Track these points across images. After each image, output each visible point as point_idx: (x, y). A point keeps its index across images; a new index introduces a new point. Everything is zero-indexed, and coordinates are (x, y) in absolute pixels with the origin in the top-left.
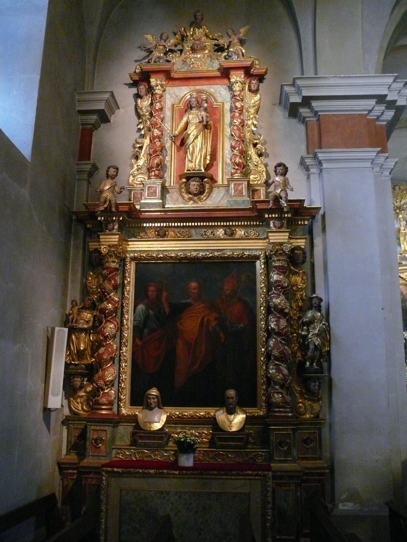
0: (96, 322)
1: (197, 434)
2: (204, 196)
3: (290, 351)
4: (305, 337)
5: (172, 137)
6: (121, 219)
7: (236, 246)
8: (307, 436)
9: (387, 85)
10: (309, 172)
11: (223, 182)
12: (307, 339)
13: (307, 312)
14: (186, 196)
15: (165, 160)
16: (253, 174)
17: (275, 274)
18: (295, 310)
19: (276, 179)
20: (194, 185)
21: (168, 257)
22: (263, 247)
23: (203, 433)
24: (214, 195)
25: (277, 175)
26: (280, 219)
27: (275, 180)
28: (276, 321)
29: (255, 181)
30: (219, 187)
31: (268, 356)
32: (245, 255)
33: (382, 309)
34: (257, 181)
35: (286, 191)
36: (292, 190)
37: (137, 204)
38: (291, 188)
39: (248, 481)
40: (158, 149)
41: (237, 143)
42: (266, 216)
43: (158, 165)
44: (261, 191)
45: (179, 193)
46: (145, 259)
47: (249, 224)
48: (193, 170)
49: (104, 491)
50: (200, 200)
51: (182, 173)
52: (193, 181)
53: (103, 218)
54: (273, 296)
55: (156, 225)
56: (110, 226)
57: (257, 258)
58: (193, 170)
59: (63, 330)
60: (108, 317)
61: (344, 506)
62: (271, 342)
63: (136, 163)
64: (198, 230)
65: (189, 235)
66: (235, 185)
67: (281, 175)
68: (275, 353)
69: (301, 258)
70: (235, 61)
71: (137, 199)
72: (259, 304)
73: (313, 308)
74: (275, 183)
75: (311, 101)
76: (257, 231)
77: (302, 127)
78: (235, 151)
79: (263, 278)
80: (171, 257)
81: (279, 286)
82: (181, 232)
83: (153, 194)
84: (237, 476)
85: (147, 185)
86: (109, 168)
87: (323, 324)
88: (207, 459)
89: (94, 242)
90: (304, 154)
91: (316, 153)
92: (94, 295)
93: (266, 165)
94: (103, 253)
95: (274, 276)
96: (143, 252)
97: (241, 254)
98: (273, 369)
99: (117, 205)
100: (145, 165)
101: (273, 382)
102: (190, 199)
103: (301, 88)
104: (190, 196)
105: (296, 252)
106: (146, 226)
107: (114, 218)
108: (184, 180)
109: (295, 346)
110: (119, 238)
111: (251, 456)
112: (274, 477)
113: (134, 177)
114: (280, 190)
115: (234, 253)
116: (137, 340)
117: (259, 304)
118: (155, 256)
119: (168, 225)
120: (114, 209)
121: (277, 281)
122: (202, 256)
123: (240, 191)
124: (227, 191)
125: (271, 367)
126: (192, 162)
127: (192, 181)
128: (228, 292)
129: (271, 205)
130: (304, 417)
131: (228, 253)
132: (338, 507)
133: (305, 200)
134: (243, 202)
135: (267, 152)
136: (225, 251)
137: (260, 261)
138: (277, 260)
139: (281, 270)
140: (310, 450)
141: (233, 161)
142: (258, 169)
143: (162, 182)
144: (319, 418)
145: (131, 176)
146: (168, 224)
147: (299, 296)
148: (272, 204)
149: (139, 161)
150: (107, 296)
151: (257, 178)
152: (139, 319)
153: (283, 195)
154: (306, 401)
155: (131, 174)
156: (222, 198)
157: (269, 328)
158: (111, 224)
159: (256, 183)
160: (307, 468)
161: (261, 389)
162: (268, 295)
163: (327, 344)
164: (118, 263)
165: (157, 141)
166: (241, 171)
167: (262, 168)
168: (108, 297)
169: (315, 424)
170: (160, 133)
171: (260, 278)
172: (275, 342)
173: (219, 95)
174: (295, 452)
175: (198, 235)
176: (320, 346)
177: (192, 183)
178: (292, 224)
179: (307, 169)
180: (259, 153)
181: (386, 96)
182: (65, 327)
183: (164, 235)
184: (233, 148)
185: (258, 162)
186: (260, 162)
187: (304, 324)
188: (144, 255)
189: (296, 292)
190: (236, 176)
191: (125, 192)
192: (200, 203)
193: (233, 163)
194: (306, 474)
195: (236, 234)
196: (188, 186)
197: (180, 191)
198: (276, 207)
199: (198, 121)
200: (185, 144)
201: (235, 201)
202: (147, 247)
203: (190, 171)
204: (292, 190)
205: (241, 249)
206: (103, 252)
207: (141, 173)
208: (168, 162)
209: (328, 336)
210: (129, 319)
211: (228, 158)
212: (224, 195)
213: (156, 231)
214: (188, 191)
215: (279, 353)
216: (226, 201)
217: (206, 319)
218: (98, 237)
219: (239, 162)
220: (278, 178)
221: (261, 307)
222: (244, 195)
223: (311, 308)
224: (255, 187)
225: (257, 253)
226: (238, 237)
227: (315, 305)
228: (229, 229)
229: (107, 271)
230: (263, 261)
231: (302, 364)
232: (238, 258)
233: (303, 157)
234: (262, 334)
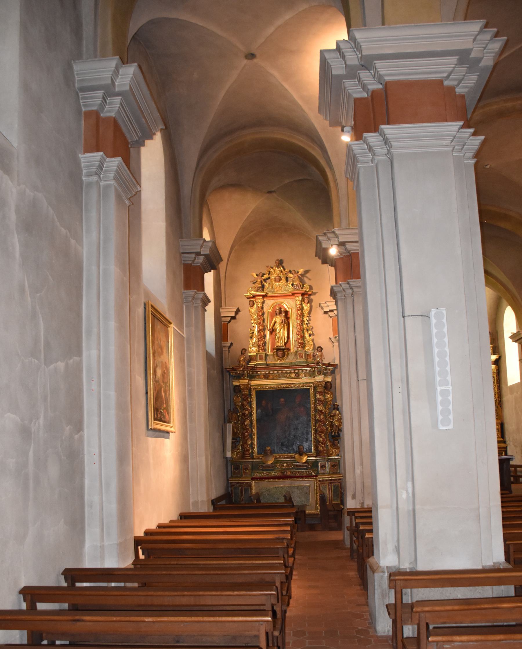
3: (325, 429)
4: (332, 422)
14: (277, 358)
36: (324, 359)
50: (283, 359)
52: (280, 351)
56: (244, 376)
59: (230, 425)
62: (317, 425)
67: (320, 351)
68: (319, 429)
69: (330, 387)
75: (375, 62)
81: (320, 400)
91: (349, 282)
98: (318, 436)
102: (278, 359)
105: (327, 384)
108: (275, 351)
121: (319, 398)
126: (279, 342)
139: (321, 393)
153: (320, 361)
156: (293, 358)
167: (311, 343)
171: (312, 397)
187: (331, 416)
197: (274, 356)
204: (324, 359)
210: (255, 417)
223: (334, 409)
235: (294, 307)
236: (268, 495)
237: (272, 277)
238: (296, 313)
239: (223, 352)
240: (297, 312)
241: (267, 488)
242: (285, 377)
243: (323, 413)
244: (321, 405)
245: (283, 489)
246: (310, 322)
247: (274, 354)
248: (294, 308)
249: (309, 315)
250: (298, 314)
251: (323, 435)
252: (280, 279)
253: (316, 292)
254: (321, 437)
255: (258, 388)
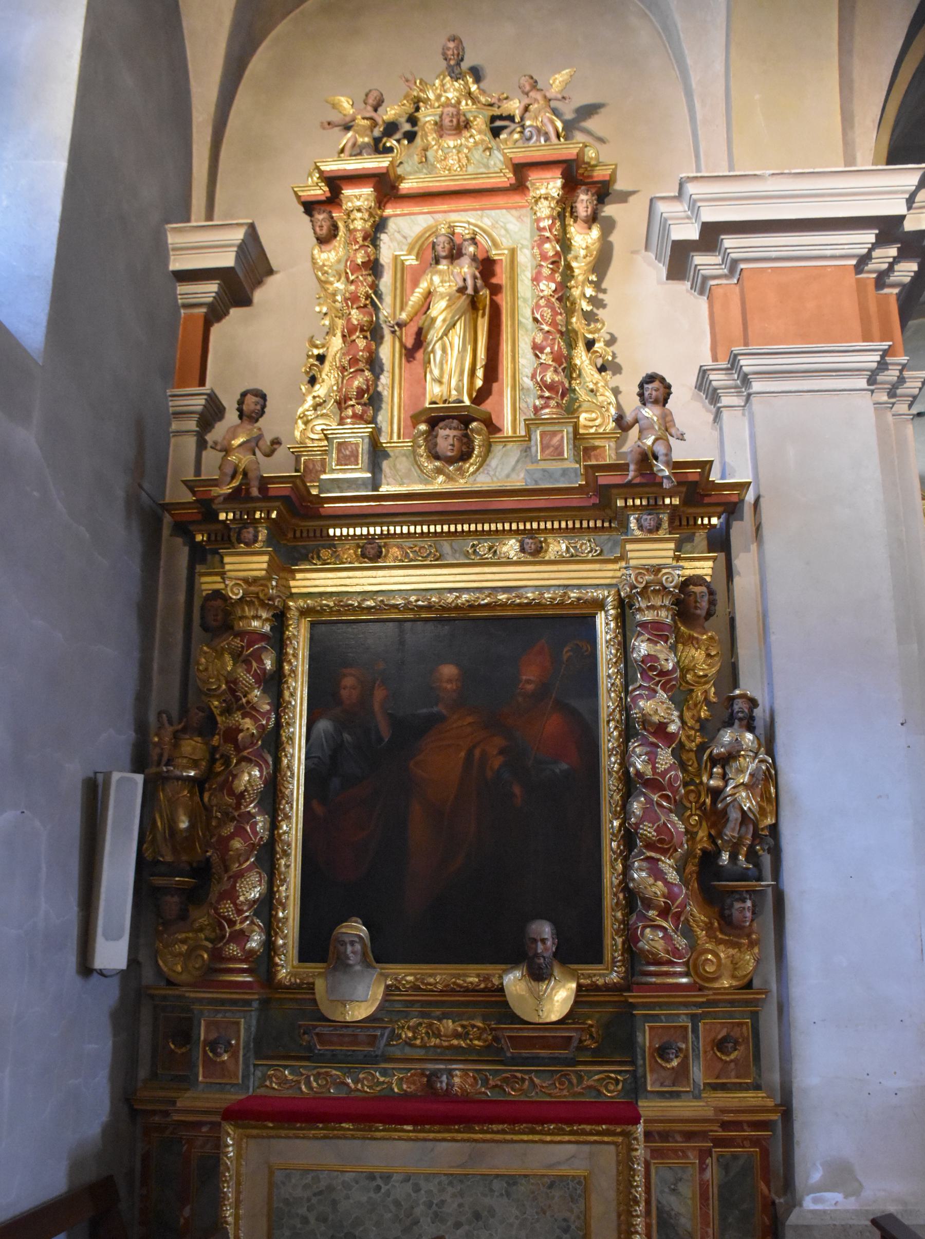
0: (218, 764)
1: (460, 1029)
2: (472, 464)
4: (716, 793)
5: (393, 327)
6: (274, 515)
7: (548, 579)
8: (723, 1033)
9: (903, 192)
10: (719, 405)
11: (514, 431)
12: (722, 796)
13: (722, 732)
14: (429, 465)
15: (379, 383)
16: (586, 412)
17: (642, 641)
18: (692, 728)
19: (643, 412)
20: (447, 437)
21: (386, 605)
22: (614, 581)
23: (473, 1026)
24: (494, 462)
25: (644, 404)
26: (653, 508)
27: (640, 416)
28: (646, 754)
29: (592, 427)
30: (506, 441)
31: (629, 838)
32: (569, 598)
33: (902, 724)
34: (597, 426)
35: (668, 441)
36: (681, 437)
37: (314, 486)
38: (679, 433)
39: (586, 1148)
40: (362, 356)
41: (548, 338)
42: (620, 503)
43: (361, 393)
44: (605, 451)
45: (412, 458)
46: (332, 612)
47: (578, 525)
48: (445, 402)
49: (229, 1173)
50: (462, 472)
51: (420, 409)
53: (231, 516)
54: (638, 692)
55: (358, 531)
56: (248, 533)
57: (600, 605)
58: (445, 402)
60: (245, 749)
61: (815, 1201)
62: (635, 805)
63: (310, 392)
64: (458, 543)
65: (435, 555)
66: (543, 434)
67: (656, 402)
68: (648, 830)
69: (704, 604)
70: (538, 150)
71: (313, 475)
72: (603, 715)
73: (736, 721)
74: (641, 422)
76: (597, 543)
77: (703, 302)
78: (543, 357)
79: (613, 651)
80: (395, 606)
81: (652, 668)
82: (417, 549)
83: (349, 459)
84: (558, 1134)
85: (336, 438)
86: (244, 395)
87: (761, 761)
88: (483, 1089)
89: (210, 574)
90: (707, 361)
92: (211, 700)
93: (616, 392)
94: (231, 598)
95: (640, 645)
96: (327, 596)
97: (561, 596)
99: (264, 482)
100: (332, 394)
101: (642, 902)
102: (439, 471)
103: (699, 204)
104: (437, 464)
106: (335, 535)
107: (257, 515)
109: (691, 815)
110: (270, 563)
111: (590, 1083)
112: (648, 1135)
113: (306, 423)
114: (653, 437)
115: (543, 594)
116: (315, 803)
117: (605, 716)
118: (356, 604)
119: (385, 532)
120: (255, 492)
121: (650, 657)
122: (467, 601)
123: (556, 449)
124: (526, 451)
125: (636, 864)
126: (440, 382)
127: (441, 429)
128: (530, 687)
129: (631, 474)
130: (716, 985)
131: (529, 595)
132: (801, 1205)
133: (712, 461)
134: (565, 472)
135: (617, 360)
136: (522, 591)
137: (606, 612)
138: (648, 608)
139: (656, 631)
140: (732, 1065)
141: (539, 379)
142: (597, 400)
143: (370, 430)
144: (752, 989)
145: (300, 422)
146: (385, 528)
147: (699, 695)
148: (635, 471)
149: (317, 387)
150: (241, 699)
151: (595, 420)
152: (319, 754)
153: (660, 449)
154: (722, 947)
155: (300, 418)
156: (513, 469)
157: (631, 769)
158: (251, 530)
159: (592, 431)
160: (724, 1111)
161: (612, 917)
162: (627, 693)
163: (769, 808)
164: (267, 620)
165: (358, 337)
166: (557, 403)
168: (244, 700)
169: (747, 1003)
170: (365, 319)
171: (606, 652)
172: (646, 803)
173: (503, 232)
174: (698, 1073)
175: (457, 555)
176: (754, 815)
177: (442, 433)
178: (681, 525)
179: (713, 396)
180: (600, 362)
181: (903, 217)
182: (136, 770)
183: (378, 556)
184: (537, 349)
185: (596, 384)
186: (601, 384)
188: (332, 604)
189: (693, 685)
190: (546, 413)
191: (281, 452)
192: (462, 481)
193: (538, 384)
194: (725, 1125)
195: (546, 551)
196: (433, 441)
198: (644, 481)
199: (455, 288)
200: (425, 344)
201: (544, 470)
202: (338, 584)
203: (435, 403)
204: (681, 437)
205: (559, 586)
206: (231, 595)
207: (322, 415)
208: (386, 388)
209: (773, 790)
211: (527, 377)
212: (518, 461)
213: (358, 546)
214: (433, 452)
215: (655, 831)
216: (522, 475)
217: (477, 752)
218: (222, 564)
219: (553, 381)
220: (647, 409)
221: (608, 722)
222: (566, 456)
224: (592, 441)
225: (600, 594)
226: (553, 558)
227: (740, 715)
228: (531, 538)
229: (242, 641)
230: (612, 612)
231: (709, 859)
232: (552, 606)
233: (705, 368)
234: (610, 786)
235: (526, 243)
236: (325, 1220)
237: (427, 117)
238: (534, 256)
239: (173, 440)
240: (540, 246)
241: (317, 1179)
242: (467, 554)
243: (669, 738)
244: (662, 695)
245: (417, 1189)
246: (601, 313)
247: (415, 446)
248: (523, 246)
249: (601, 278)
250: (544, 257)
251: (667, 865)
252: (462, 126)
253: (630, 189)
254: (658, 874)
255: (321, 612)
